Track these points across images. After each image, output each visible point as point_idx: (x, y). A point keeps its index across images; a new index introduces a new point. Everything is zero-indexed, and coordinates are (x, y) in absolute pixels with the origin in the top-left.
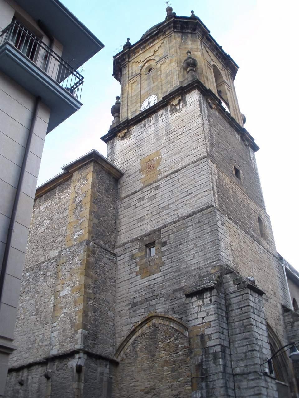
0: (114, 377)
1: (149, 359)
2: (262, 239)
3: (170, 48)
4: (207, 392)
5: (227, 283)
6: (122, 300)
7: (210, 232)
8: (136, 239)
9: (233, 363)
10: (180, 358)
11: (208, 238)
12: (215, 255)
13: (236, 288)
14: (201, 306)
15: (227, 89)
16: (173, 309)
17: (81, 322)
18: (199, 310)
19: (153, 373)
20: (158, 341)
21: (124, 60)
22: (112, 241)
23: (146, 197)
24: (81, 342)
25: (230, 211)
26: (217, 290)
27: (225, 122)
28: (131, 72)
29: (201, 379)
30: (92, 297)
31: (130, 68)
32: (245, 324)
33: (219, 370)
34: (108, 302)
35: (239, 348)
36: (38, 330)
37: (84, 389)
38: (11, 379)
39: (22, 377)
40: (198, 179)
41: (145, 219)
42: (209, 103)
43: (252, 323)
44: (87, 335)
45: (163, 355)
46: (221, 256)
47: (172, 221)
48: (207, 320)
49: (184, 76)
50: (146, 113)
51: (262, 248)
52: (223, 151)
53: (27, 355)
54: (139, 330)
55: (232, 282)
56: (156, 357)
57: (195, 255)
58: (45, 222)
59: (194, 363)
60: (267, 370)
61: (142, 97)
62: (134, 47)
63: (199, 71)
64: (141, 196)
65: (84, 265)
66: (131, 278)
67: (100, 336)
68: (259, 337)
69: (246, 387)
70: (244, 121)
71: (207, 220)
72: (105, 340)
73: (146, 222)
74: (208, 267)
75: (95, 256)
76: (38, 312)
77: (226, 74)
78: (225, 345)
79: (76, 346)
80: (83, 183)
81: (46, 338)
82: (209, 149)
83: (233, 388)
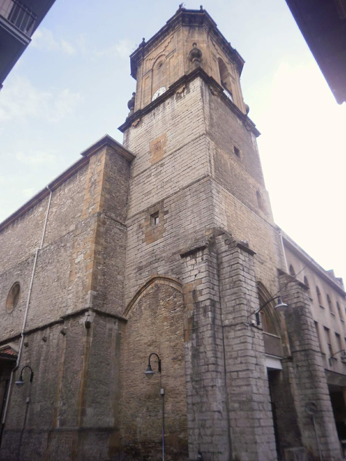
0: (122, 333)
1: (152, 315)
2: (260, 210)
3: (178, 42)
4: (197, 342)
5: (219, 243)
6: (130, 265)
7: (205, 199)
8: (143, 211)
9: (222, 316)
10: (178, 314)
11: (203, 205)
12: (209, 218)
13: (227, 247)
14: (193, 265)
15: (231, 82)
16: (172, 270)
17: (90, 285)
18: (192, 268)
19: (155, 328)
20: (159, 299)
21: (139, 58)
22: (123, 215)
23: (153, 174)
24: (90, 302)
25: (227, 182)
26: (208, 249)
27: (227, 108)
28: (144, 69)
29: (192, 331)
30: (102, 262)
31: (145, 65)
32: (234, 280)
33: (208, 322)
34: (117, 267)
35: (229, 302)
36: (58, 294)
37: (92, 342)
38: (37, 337)
39: (45, 335)
40: (196, 154)
41: (151, 192)
42: (211, 90)
43: (241, 279)
44: (96, 295)
45: (163, 312)
46: (214, 220)
47: (174, 192)
48: (199, 277)
49: (189, 66)
50: (156, 102)
51: (259, 218)
52: (223, 132)
53: (49, 316)
54: (144, 291)
55: (223, 243)
56: (157, 314)
57: (192, 220)
58: (67, 202)
59: (187, 316)
60: (254, 322)
61: (153, 89)
62: (147, 45)
63: (204, 62)
64: (149, 173)
65: (95, 234)
66: (138, 245)
67: (109, 296)
68: (247, 292)
69: (233, 336)
70: (247, 110)
71: (203, 188)
72: (114, 300)
73: (152, 195)
74: (203, 230)
75: (106, 226)
76: (59, 279)
77: (232, 68)
78: (216, 300)
79: (86, 306)
80: (98, 164)
81: (64, 300)
82: (208, 128)
83: (222, 338)
